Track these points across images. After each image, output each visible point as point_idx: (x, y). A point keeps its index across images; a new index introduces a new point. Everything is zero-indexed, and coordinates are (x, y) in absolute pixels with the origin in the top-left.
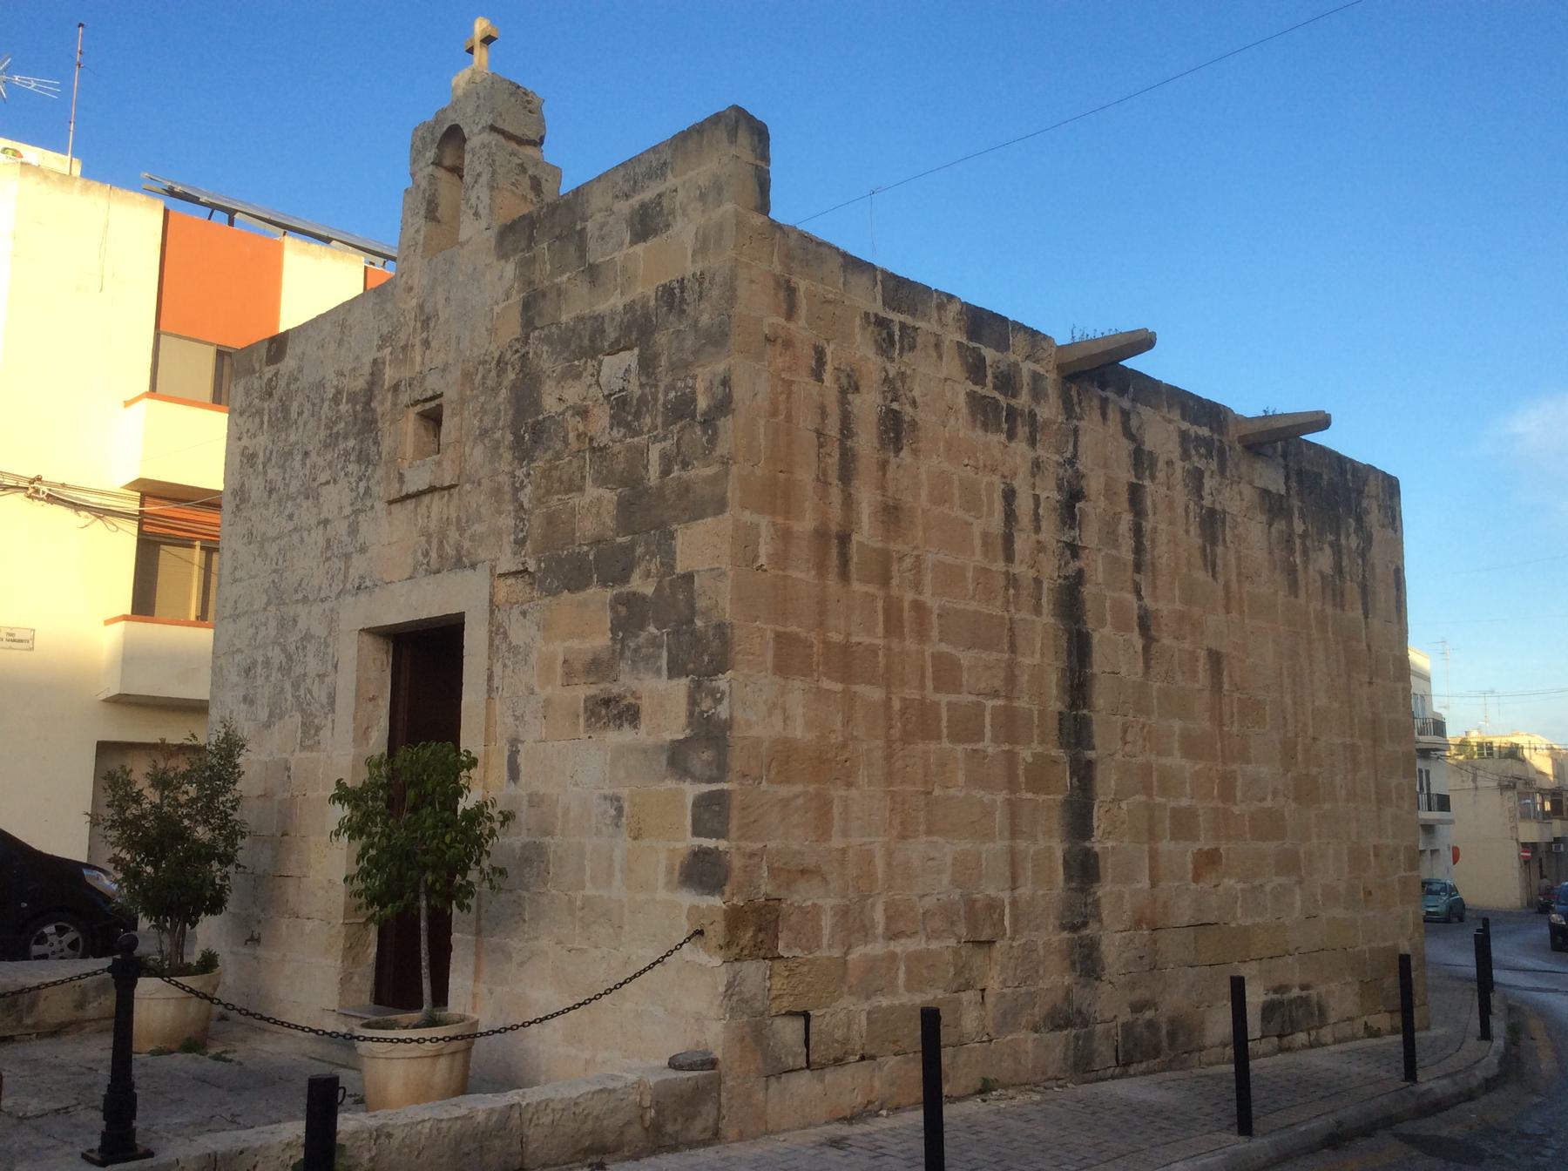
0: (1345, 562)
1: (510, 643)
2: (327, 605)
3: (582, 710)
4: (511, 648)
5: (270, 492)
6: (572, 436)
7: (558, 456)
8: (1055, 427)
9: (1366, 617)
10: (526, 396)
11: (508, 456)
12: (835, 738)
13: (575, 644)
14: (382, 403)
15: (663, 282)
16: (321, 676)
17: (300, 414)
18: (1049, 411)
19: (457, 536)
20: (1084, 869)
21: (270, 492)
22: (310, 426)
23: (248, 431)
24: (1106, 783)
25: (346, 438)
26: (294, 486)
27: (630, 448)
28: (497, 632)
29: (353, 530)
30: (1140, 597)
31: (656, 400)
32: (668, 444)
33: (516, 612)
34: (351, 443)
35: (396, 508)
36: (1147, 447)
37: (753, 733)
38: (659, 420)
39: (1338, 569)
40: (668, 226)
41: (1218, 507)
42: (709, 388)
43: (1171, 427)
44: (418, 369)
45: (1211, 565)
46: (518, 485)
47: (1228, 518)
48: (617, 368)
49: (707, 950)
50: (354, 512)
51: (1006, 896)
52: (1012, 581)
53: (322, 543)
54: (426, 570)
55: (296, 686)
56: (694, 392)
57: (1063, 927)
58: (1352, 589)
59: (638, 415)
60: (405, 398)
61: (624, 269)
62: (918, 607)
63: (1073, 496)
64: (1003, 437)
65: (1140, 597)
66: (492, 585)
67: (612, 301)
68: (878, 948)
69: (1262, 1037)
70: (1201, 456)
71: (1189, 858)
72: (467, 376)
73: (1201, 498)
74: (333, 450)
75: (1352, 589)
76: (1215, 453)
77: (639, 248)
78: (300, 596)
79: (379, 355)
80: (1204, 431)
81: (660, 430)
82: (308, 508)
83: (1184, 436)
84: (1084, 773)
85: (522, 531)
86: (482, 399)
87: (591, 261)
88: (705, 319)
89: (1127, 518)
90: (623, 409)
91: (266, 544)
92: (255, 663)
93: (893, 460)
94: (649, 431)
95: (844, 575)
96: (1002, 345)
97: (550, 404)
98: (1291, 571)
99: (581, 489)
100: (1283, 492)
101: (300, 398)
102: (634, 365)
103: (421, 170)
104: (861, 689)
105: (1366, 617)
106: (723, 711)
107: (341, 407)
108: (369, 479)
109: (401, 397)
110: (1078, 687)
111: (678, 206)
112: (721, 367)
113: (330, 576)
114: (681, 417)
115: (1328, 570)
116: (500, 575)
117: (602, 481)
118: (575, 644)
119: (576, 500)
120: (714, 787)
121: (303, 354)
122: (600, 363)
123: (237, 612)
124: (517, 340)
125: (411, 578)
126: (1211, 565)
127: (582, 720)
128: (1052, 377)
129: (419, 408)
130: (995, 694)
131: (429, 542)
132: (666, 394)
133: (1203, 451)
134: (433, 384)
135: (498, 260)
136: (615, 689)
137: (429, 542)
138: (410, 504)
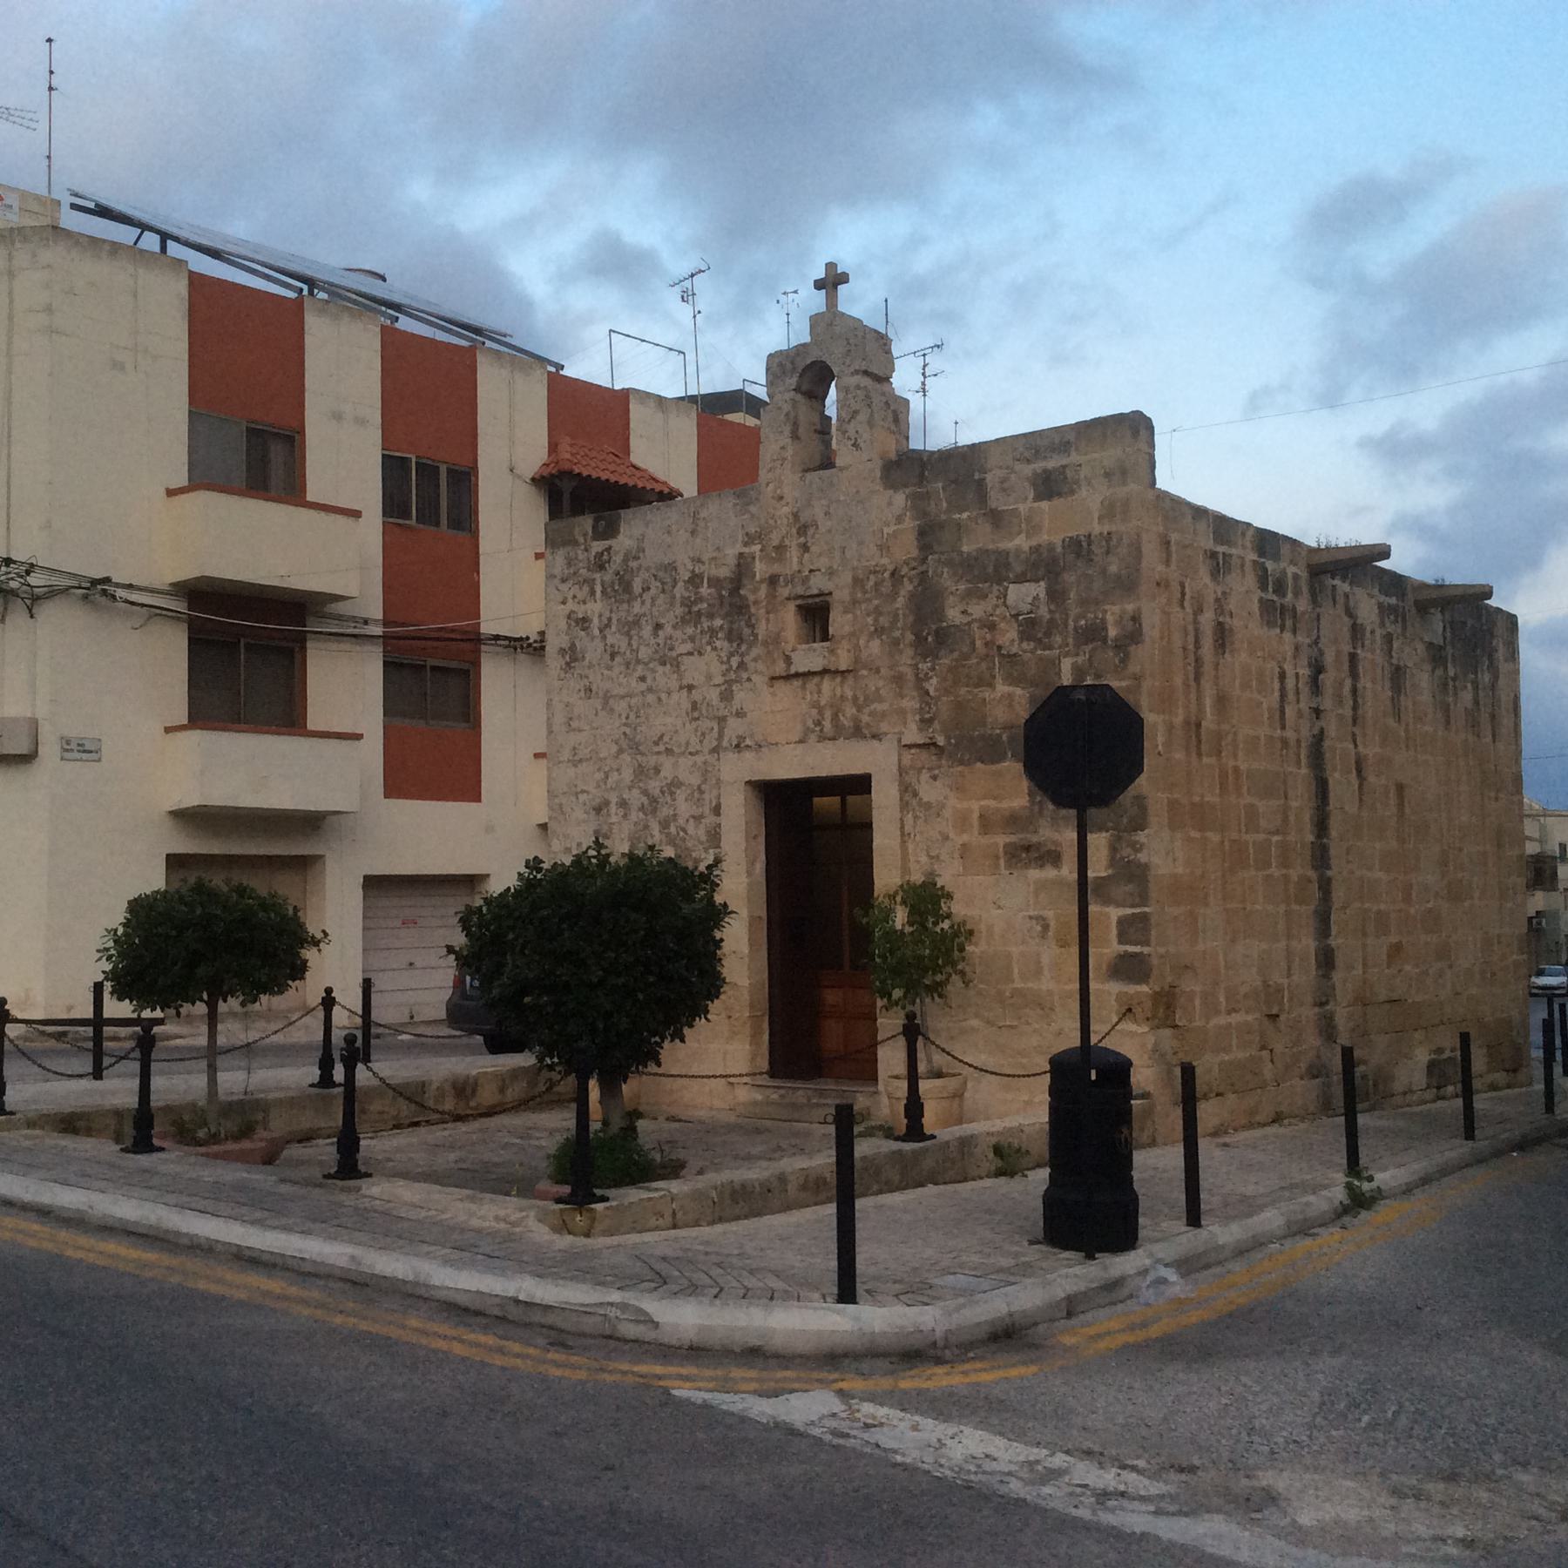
0: (1481, 694)
1: (921, 799)
2: (699, 759)
3: (1001, 854)
4: (920, 803)
5: (613, 656)
6: (979, 643)
7: (966, 657)
8: (1307, 616)
9: (1494, 742)
10: (926, 603)
11: (910, 652)
12: (1198, 872)
13: (992, 803)
14: (755, 591)
15: (1070, 535)
16: (698, 818)
17: (646, 589)
18: (1303, 605)
19: (854, 710)
20: (1326, 960)
21: (613, 656)
22: (659, 601)
23: (575, 597)
24: (1338, 894)
25: (711, 616)
26: (644, 653)
27: (1041, 659)
28: (907, 790)
29: (727, 696)
30: (1356, 746)
31: (1066, 626)
32: (1080, 659)
33: (925, 776)
34: (718, 622)
35: (779, 684)
36: (1359, 621)
37: (1160, 872)
38: (1070, 640)
39: (1476, 702)
40: (1072, 492)
41: (1402, 664)
42: (1119, 622)
43: (1373, 601)
44: (795, 567)
45: (1398, 716)
46: (921, 676)
47: (1408, 670)
48: (1023, 595)
49: (1136, 1021)
50: (726, 682)
51: (1285, 981)
52: (1285, 743)
53: (686, 705)
54: (820, 737)
55: (665, 825)
56: (1104, 621)
57: (1315, 1005)
58: (1484, 717)
59: (1048, 634)
60: (784, 592)
61: (1029, 519)
62: (1236, 770)
63: (1318, 669)
64: (1278, 631)
65: (1356, 746)
66: (900, 755)
67: (1017, 541)
68: (1222, 1020)
69: (1427, 1088)
70: (1392, 623)
71: (1385, 950)
72: (857, 582)
73: (1391, 657)
74: (696, 627)
75: (1484, 717)
76: (1400, 619)
77: (1045, 505)
78: (661, 748)
79: (746, 550)
80: (1393, 601)
81: (1071, 647)
82: (664, 673)
83: (1380, 605)
84: (1325, 886)
85: (929, 712)
86: (876, 602)
87: (993, 507)
88: (1113, 569)
89: (1348, 683)
90: (1029, 627)
91: (611, 701)
92: (607, 803)
93: (1221, 661)
94: (1060, 647)
95: (1199, 755)
96: (1276, 557)
97: (953, 614)
98: (1446, 709)
99: (991, 685)
100: (1442, 644)
101: (644, 575)
102: (1042, 595)
103: (780, 392)
104: (1209, 834)
105: (1494, 742)
106: (1142, 857)
107: (701, 590)
108: (742, 655)
109: (780, 590)
110: (1321, 826)
111: (1082, 476)
112: (1130, 607)
113: (699, 734)
114: (1093, 640)
115: (1470, 705)
116: (905, 746)
117: (1011, 680)
118: (992, 803)
119: (987, 695)
120: (1137, 910)
121: (643, 535)
122: (1006, 589)
123: (576, 758)
124: (914, 559)
125: (801, 742)
126: (1398, 716)
127: (1002, 862)
128: (1304, 575)
129: (799, 602)
130: (1277, 832)
131: (821, 713)
132: (1076, 621)
133: (1392, 617)
134: (818, 584)
135: (885, 489)
136: (1035, 839)
137: (821, 713)
138: (797, 683)
